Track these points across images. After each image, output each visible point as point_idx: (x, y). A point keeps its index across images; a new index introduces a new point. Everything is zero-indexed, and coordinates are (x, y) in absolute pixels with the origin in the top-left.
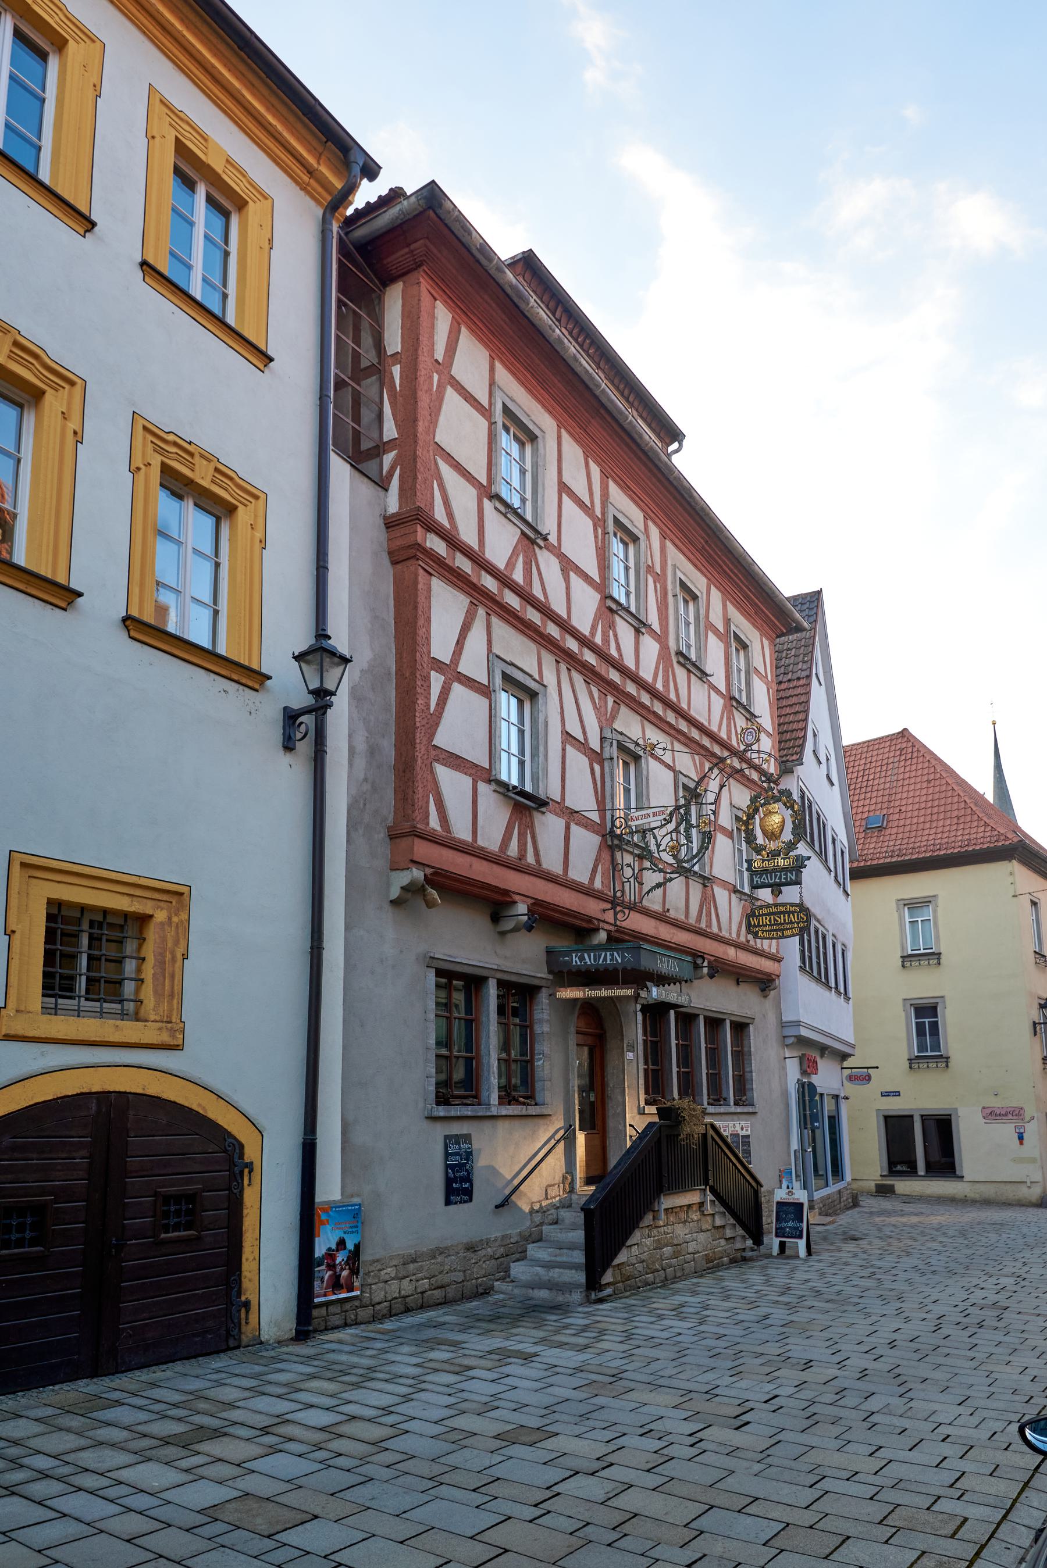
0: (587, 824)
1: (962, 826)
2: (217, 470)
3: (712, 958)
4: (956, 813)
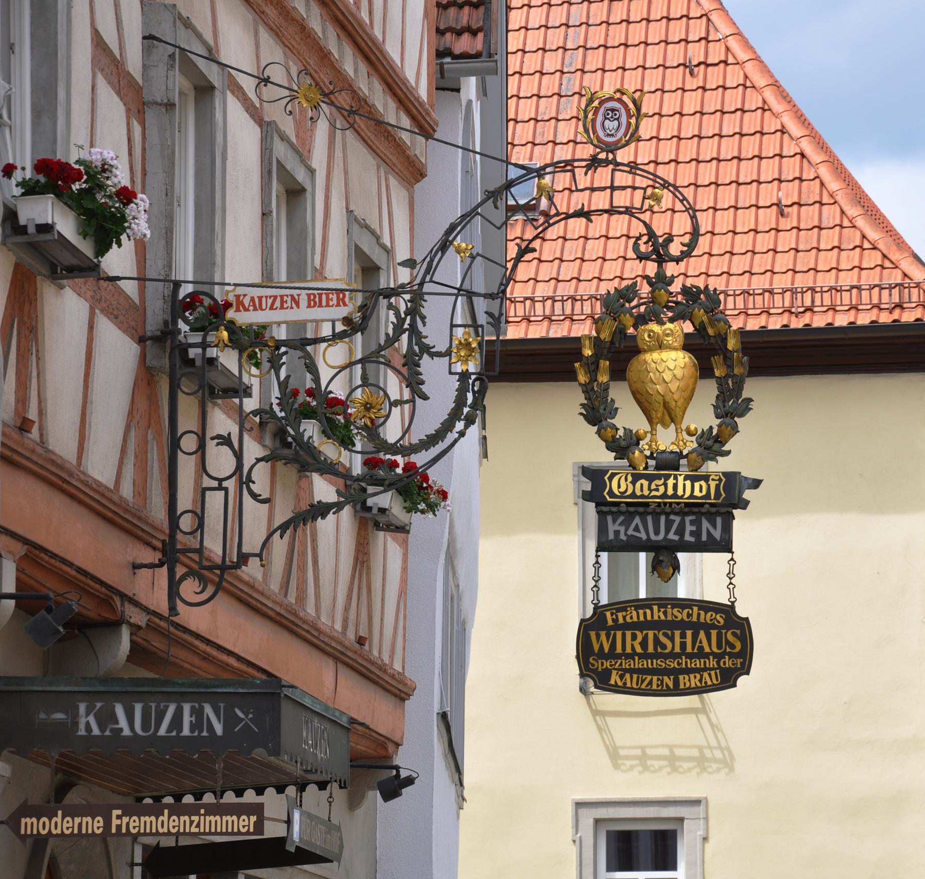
4: (768, 194)
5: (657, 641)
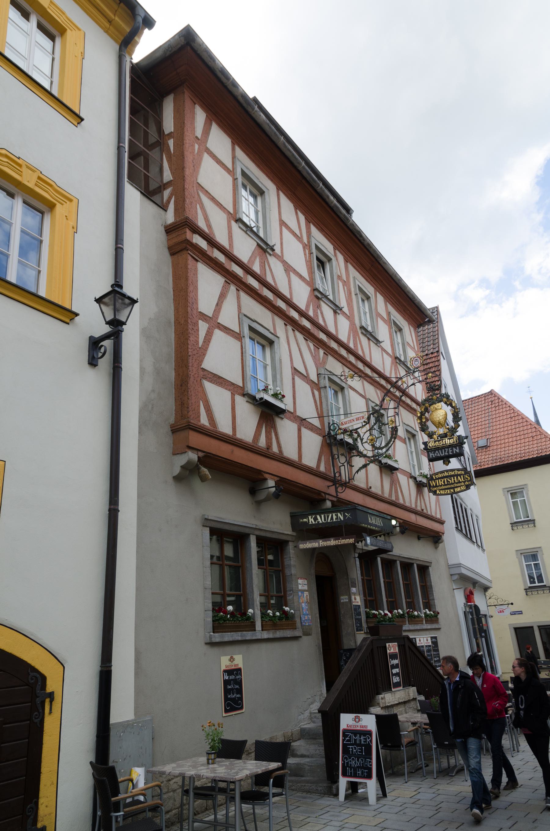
0: (312, 428)
1: (536, 442)
2: (39, 178)
3: (401, 521)
4: (531, 435)
5: (447, 481)
